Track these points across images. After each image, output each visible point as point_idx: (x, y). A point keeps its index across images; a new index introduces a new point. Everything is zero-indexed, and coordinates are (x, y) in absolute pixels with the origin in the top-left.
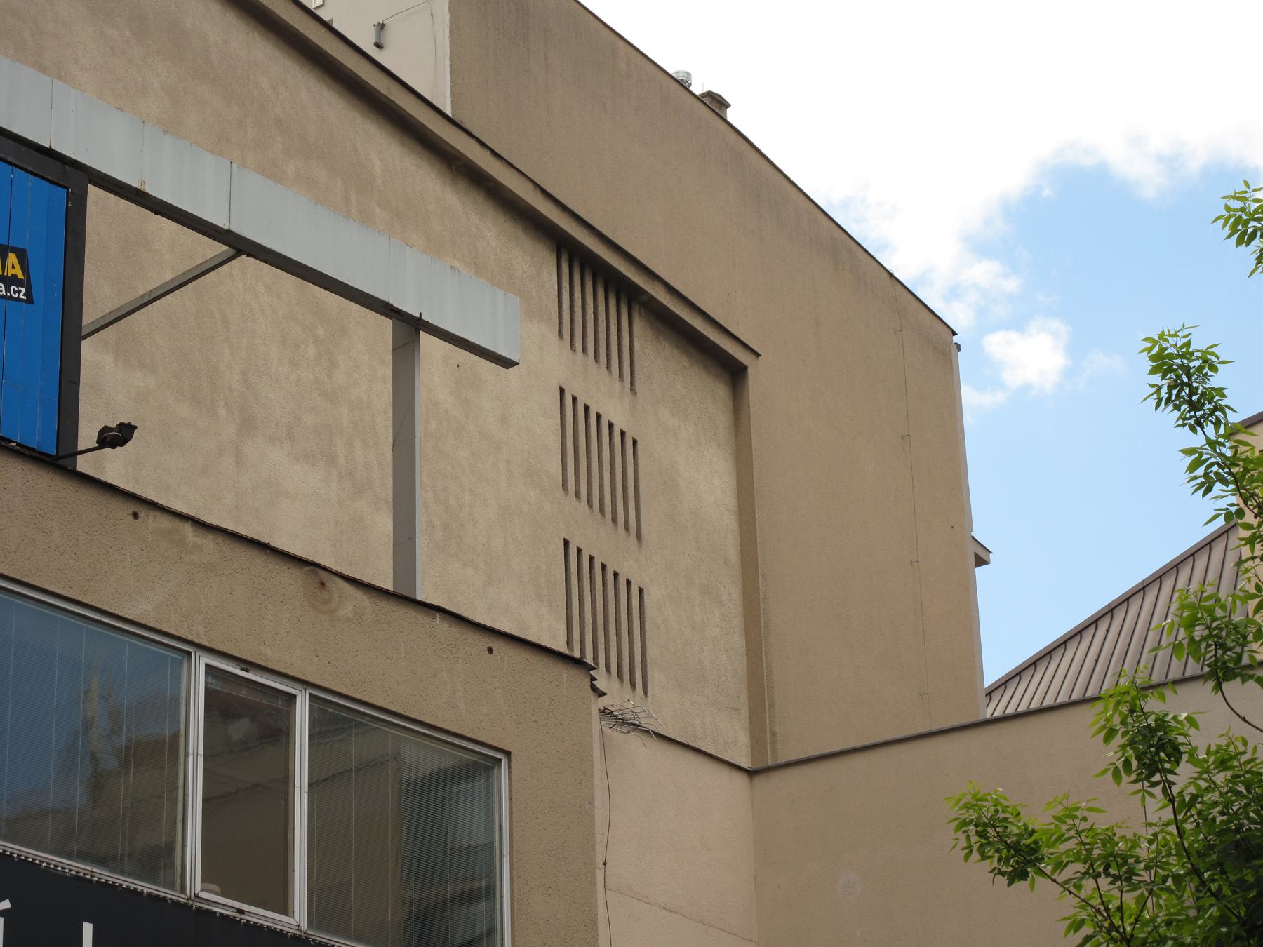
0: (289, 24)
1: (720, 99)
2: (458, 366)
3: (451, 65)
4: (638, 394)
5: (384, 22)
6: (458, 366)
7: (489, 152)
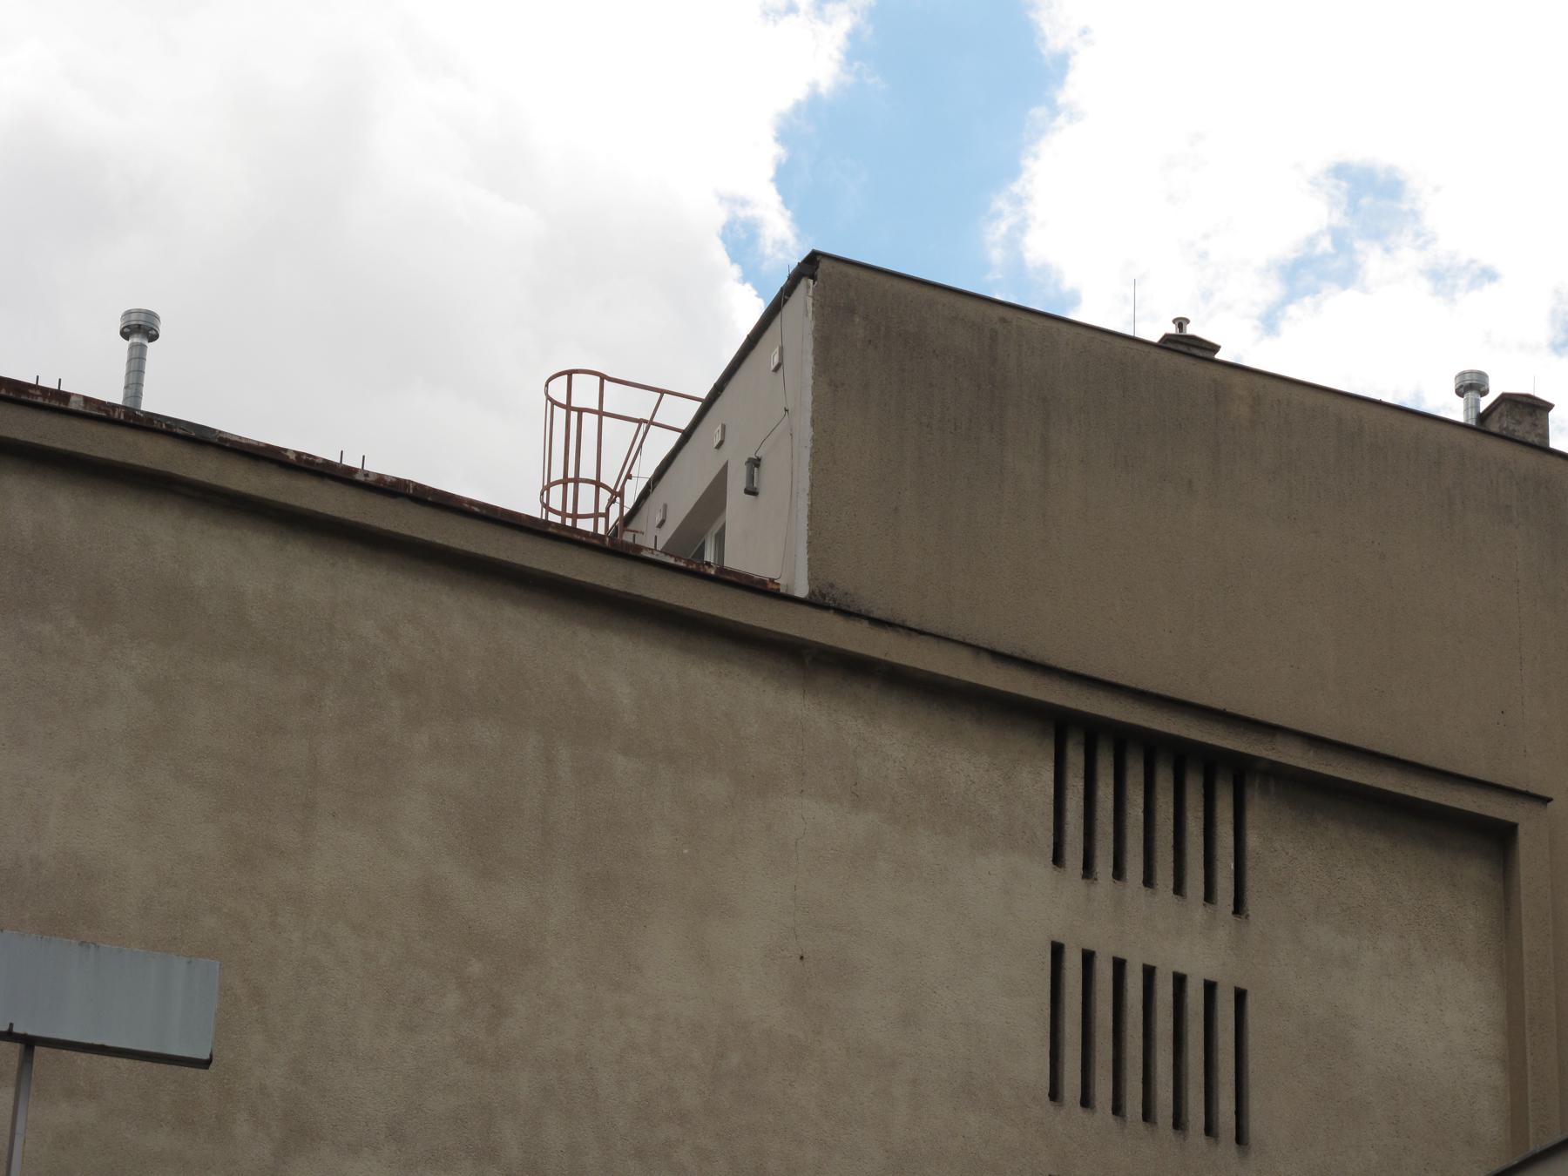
0: (404, 536)
1: (1530, 401)
2: (802, 958)
3: (811, 506)
4: (1250, 918)
5: (759, 455)
6: (802, 958)
7: (866, 624)
